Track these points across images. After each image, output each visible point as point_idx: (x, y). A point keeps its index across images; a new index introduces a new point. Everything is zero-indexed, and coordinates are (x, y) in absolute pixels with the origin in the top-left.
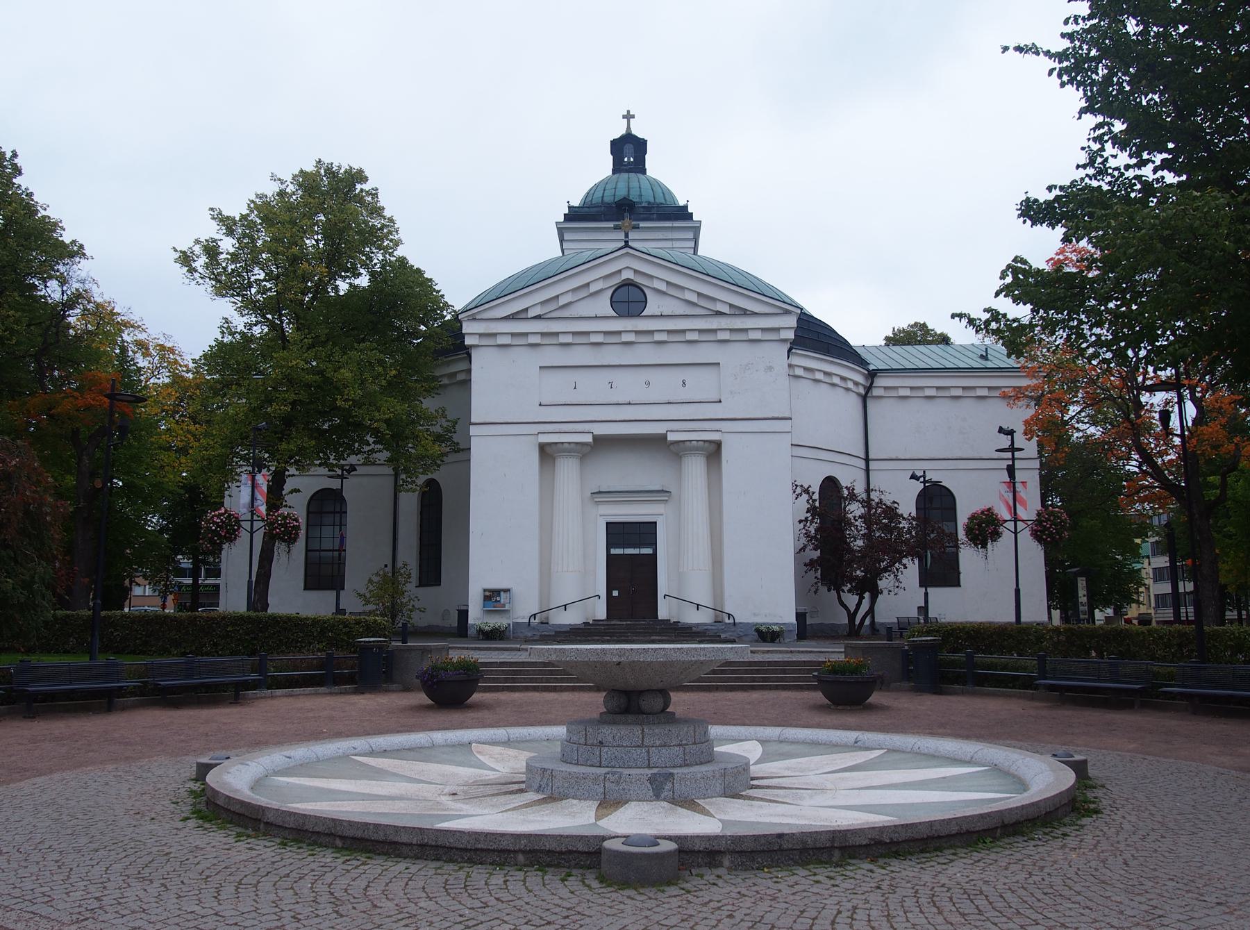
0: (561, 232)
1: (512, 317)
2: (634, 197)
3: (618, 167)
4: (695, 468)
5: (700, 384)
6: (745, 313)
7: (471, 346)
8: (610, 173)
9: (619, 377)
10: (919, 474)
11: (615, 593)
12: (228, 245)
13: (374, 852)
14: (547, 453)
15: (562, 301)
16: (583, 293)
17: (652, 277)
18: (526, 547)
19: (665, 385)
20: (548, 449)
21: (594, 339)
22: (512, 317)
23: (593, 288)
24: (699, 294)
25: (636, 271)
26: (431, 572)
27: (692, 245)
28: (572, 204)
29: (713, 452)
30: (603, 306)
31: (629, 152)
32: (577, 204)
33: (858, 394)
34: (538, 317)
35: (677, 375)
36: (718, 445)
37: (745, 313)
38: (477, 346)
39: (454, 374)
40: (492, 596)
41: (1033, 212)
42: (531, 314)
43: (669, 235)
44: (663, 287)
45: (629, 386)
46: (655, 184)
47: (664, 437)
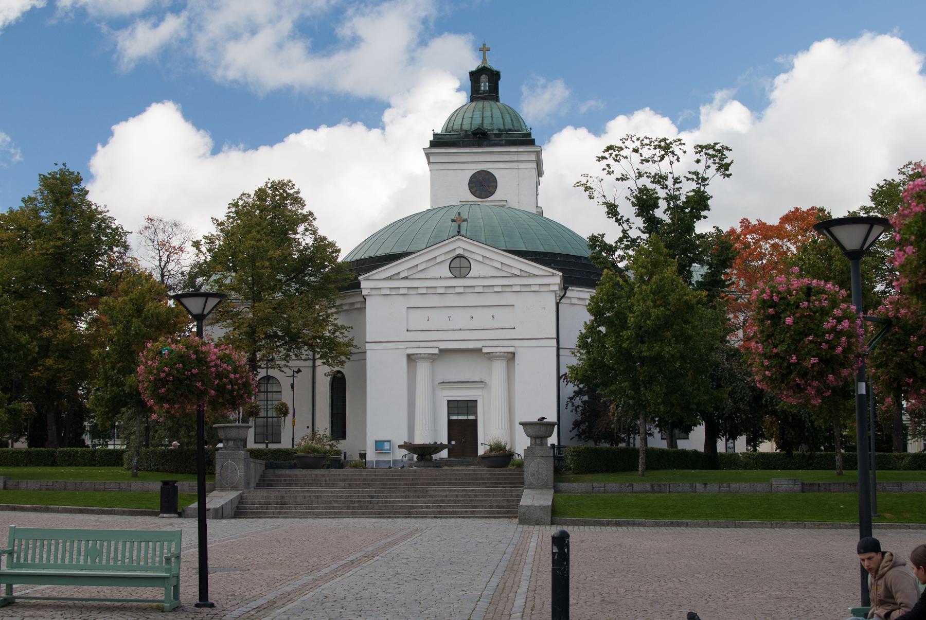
0: (428, 155)
1: (389, 278)
2: (487, 126)
3: (476, 95)
4: (499, 367)
5: (503, 318)
6: (530, 275)
9: (454, 313)
11: (453, 443)
15: (420, 268)
16: (433, 263)
18: (395, 414)
19: (482, 318)
20: (412, 357)
21: (439, 291)
22: (389, 278)
23: (438, 260)
26: (339, 428)
28: (436, 132)
29: (511, 357)
30: (445, 271)
32: (439, 132)
34: (406, 278)
35: (490, 312)
36: (514, 354)
37: (530, 275)
40: (379, 445)
41: (705, 217)
42: (402, 276)
43: (515, 158)
44: (480, 259)
45: (460, 319)
47: (480, 350)
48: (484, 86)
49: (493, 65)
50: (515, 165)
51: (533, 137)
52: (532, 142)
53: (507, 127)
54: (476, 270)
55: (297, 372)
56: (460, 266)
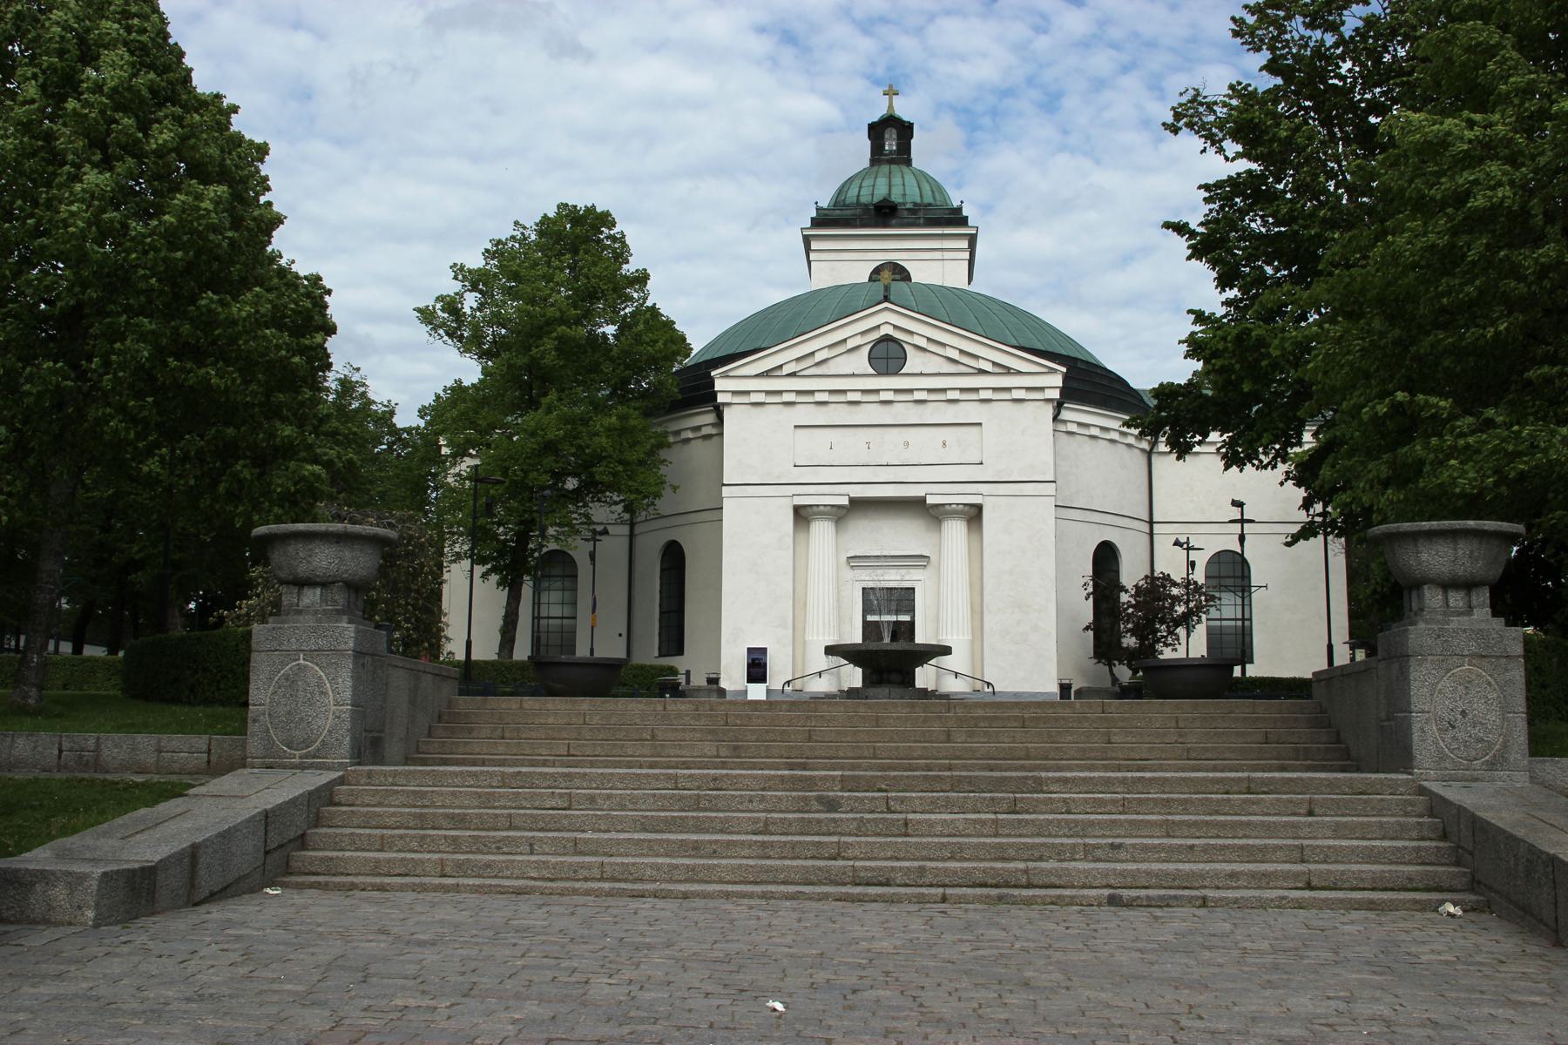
0: (807, 240)
2: (896, 197)
3: (878, 155)
4: (955, 530)
6: (1008, 371)
7: (725, 404)
8: (867, 164)
10: (1183, 539)
12: (470, 301)
13: (793, 703)
14: (802, 515)
15: (818, 357)
16: (841, 349)
17: (911, 333)
18: (775, 607)
19: (925, 444)
20: (803, 512)
23: (851, 344)
24: (961, 351)
25: (895, 327)
26: (673, 640)
27: (967, 255)
29: (974, 515)
30: (860, 362)
31: (891, 138)
32: (824, 204)
33: (1143, 450)
34: (793, 375)
37: (1008, 371)
38: (729, 404)
39: (699, 428)
42: (786, 370)
44: (923, 343)
45: (890, 445)
46: (921, 177)
48: (890, 145)
49: (903, 110)
50: (938, 255)
51: (965, 213)
52: (963, 222)
53: (926, 201)
54: (914, 362)
55: (601, 533)
56: (888, 355)
